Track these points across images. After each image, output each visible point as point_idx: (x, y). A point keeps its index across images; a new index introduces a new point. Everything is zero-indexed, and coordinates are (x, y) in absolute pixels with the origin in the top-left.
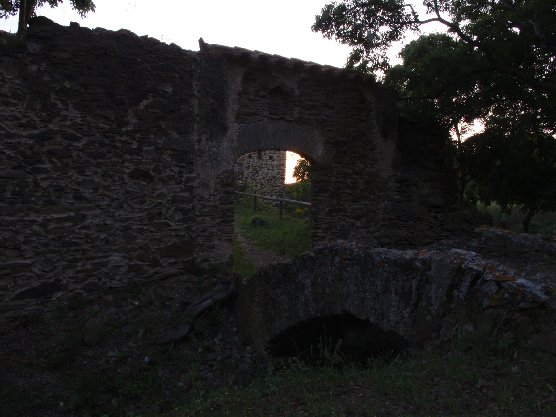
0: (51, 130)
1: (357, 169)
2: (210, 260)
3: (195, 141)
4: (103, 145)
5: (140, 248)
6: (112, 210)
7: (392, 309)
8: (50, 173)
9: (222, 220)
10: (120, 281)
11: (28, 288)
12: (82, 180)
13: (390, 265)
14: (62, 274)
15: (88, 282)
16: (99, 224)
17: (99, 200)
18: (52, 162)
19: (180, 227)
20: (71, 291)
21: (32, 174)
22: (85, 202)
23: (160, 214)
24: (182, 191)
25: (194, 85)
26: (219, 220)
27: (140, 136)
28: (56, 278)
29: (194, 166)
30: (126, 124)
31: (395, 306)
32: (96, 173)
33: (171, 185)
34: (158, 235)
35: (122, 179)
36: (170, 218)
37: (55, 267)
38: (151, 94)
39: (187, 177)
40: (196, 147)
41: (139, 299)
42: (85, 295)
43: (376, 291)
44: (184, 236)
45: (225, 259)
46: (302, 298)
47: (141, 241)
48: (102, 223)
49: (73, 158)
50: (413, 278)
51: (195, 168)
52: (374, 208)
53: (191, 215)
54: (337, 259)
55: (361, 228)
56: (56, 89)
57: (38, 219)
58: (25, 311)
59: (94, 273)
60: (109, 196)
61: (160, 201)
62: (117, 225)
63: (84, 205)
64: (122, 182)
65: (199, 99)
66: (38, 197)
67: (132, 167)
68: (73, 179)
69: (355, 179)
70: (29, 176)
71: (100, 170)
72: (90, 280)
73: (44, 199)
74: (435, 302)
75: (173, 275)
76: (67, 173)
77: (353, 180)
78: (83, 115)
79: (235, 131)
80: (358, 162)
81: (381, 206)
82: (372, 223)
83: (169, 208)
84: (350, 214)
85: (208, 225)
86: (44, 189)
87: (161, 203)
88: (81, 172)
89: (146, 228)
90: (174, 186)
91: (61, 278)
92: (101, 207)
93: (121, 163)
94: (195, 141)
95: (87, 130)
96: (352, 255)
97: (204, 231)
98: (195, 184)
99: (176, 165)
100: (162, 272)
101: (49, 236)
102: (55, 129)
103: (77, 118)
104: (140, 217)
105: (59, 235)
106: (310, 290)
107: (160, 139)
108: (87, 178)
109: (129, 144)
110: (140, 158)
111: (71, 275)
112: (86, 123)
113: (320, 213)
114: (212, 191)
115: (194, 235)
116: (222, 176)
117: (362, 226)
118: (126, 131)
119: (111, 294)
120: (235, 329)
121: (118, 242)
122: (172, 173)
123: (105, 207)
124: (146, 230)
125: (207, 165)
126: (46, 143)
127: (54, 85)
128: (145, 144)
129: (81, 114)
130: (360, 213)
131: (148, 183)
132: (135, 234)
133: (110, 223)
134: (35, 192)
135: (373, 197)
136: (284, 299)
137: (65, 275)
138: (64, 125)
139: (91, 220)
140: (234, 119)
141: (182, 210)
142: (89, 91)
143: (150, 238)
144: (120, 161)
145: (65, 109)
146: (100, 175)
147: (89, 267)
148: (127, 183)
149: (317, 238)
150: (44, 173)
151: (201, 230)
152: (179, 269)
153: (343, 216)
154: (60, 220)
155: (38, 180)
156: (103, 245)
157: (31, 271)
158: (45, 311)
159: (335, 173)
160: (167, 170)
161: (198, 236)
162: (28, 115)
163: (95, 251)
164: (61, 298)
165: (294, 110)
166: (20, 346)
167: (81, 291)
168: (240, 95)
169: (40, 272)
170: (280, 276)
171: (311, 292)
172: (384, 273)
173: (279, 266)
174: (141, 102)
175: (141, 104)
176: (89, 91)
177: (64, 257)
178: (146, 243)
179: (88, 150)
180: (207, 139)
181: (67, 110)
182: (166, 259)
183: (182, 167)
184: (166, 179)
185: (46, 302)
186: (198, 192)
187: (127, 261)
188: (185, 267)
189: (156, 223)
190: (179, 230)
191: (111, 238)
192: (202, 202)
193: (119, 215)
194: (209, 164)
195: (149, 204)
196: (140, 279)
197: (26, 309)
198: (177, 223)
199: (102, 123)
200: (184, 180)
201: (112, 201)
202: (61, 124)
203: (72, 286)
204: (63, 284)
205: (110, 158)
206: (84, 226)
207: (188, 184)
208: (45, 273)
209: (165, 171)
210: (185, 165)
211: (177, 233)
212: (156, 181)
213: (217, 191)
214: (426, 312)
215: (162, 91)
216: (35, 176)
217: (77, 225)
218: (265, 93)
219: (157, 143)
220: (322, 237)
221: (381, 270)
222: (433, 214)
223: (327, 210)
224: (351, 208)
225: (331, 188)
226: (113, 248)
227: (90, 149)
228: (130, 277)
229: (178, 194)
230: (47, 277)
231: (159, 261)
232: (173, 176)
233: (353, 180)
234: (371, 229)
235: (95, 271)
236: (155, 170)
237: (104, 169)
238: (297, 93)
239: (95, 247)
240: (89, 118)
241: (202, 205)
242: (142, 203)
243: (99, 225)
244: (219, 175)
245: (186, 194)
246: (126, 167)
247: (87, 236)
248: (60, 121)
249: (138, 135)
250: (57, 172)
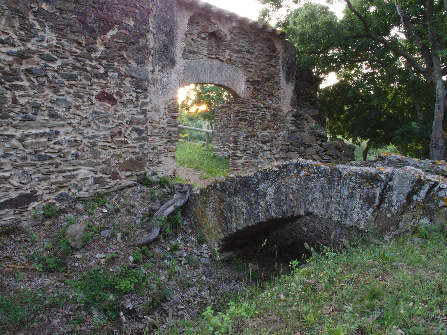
0: (29, 49)
1: (267, 104)
2: (158, 173)
3: (149, 71)
4: (75, 68)
5: (103, 162)
6: (81, 128)
7: (356, 210)
8: (28, 91)
9: (169, 140)
10: (87, 191)
11: (7, 199)
12: (57, 99)
13: (356, 178)
14: (37, 185)
15: (60, 192)
16: (70, 140)
17: (71, 118)
18: (29, 80)
19: (135, 145)
20: (45, 201)
21: (11, 90)
22: (59, 119)
23: (120, 133)
24: (139, 113)
25: (150, 22)
26: (166, 140)
27: (107, 63)
28: (32, 189)
29: (147, 93)
30: (95, 50)
31: (358, 208)
32: (69, 93)
33: (130, 108)
34: (118, 151)
35: (91, 101)
36: (128, 137)
37: (32, 179)
38: (116, 26)
39: (142, 102)
40: (150, 77)
41: (106, 207)
42: (57, 204)
43: (341, 197)
44: (138, 153)
45: (170, 173)
46: (263, 203)
47: (105, 156)
48: (73, 139)
49: (49, 78)
50: (377, 187)
51: (149, 94)
52: (276, 136)
53: (144, 135)
54: (303, 173)
55: (267, 150)
56: (34, 10)
57: (16, 134)
58: (4, 220)
59: (65, 184)
60: (79, 115)
61: (121, 122)
62: (85, 141)
63: (58, 123)
64: (90, 102)
65: (154, 34)
66: (16, 113)
67: (99, 90)
68: (49, 97)
69: (265, 112)
70: (8, 92)
71: (72, 91)
72: (62, 191)
73: (22, 115)
74: (396, 204)
75: (129, 186)
76: (43, 92)
77: (263, 112)
78: (59, 39)
79: (181, 65)
80: (268, 98)
81: (281, 134)
82: (274, 147)
83: (127, 128)
84: (260, 139)
85: (158, 144)
86: (22, 105)
87: (121, 123)
88: (56, 91)
89: (108, 144)
90: (132, 109)
91: (36, 189)
92: (73, 125)
93: (90, 86)
94: (149, 71)
95: (62, 53)
96: (319, 170)
97: (153, 149)
98: (148, 108)
99: (134, 91)
100: (120, 184)
101: (26, 150)
102: (32, 49)
103: (53, 40)
104: (104, 135)
105: (36, 150)
106: (272, 197)
107: (122, 66)
108: (61, 98)
109: (98, 69)
110: (106, 82)
111: (45, 187)
112: (61, 46)
113: (239, 137)
114: (162, 116)
115: (146, 152)
116: (170, 103)
117: (267, 149)
118: (95, 57)
119: (80, 203)
120: (190, 231)
121: (86, 157)
122: (131, 98)
123: (76, 125)
124: (108, 146)
125: (159, 92)
126: (24, 61)
127: (32, 6)
128: (111, 70)
129: (56, 37)
130: (267, 139)
131: (112, 105)
132: (100, 150)
133: (80, 139)
134: (14, 108)
135: (276, 127)
136: (242, 205)
137: (40, 187)
138: (41, 46)
139: (64, 137)
140: (181, 55)
141: (137, 130)
142: (64, 16)
143: (111, 154)
144: (90, 84)
145: (42, 30)
146: (72, 96)
147: (61, 180)
148: (94, 104)
149: (237, 158)
150: (22, 91)
151: (152, 148)
152: (133, 181)
153: (255, 140)
154: (36, 135)
155: (16, 96)
156: (73, 159)
157: (9, 183)
158: (22, 220)
159: (252, 106)
160: (127, 95)
161: (149, 153)
162: (6, 31)
163: (66, 164)
164: (36, 208)
165: (225, 52)
166: (8, 253)
167: (54, 201)
168: (186, 35)
169: (19, 184)
170: (239, 186)
171: (273, 199)
172: (351, 183)
173: (237, 178)
174: (108, 31)
175: (108, 34)
176: (64, 16)
177: (39, 170)
178: (109, 158)
179: (62, 72)
180: (159, 70)
181: (44, 31)
182: (123, 173)
183: (138, 93)
184: (126, 102)
185: (24, 212)
186: (150, 116)
187: (93, 174)
188: (138, 179)
189: (117, 141)
190: (135, 147)
191: (80, 153)
192: (153, 124)
193: (88, 133)
194: (160, 92)
195: (112, 124)
196: (103, 190)
197: (4, 219)
198: (134, 142)
199: (75, 47)
200: (140, 104)
201: (82, 120)
202: (39, 44)
203: (46, 197)
204: (39, 195)
205: (81, 80)
206: (58, 141)
207: (143, 108)
208: (22, 185)
209: (125, 95)
210: (141, 91)
211: (133, 150)
212: (118, 103)
213: (166, 115)
214: (387, 211)
215: (125, 24)
216: (14, 93)
217: (51, 141)
218: (205, 36)
219: (120, 70)
220: (240, 157)
221: (348, 181)
222: (319, 143)
223: (245, 135)
224: (261, 134)
225: (248, 118)
226: (82, 162)
227: (64, 71)
228: (95, 188)
229: (135, 116)
230: (25, 188)
231: (118, 174)
232: (132, 100)
233: (263, 112)
234: (273, 152)
235: (66, 183)
236: (118, 94)
237: (76, 90)
238: (229, 38)
239: (66, 161)
240: (63, 41)
241: (153, 126)
242: (107, 122)
243: (71, 141)
244: (168, 102)
245: (141, 117)
246: (94, 89)
247: (59, 151)
248: (37, 41)
249: (104, 62)
250: (35, 90)
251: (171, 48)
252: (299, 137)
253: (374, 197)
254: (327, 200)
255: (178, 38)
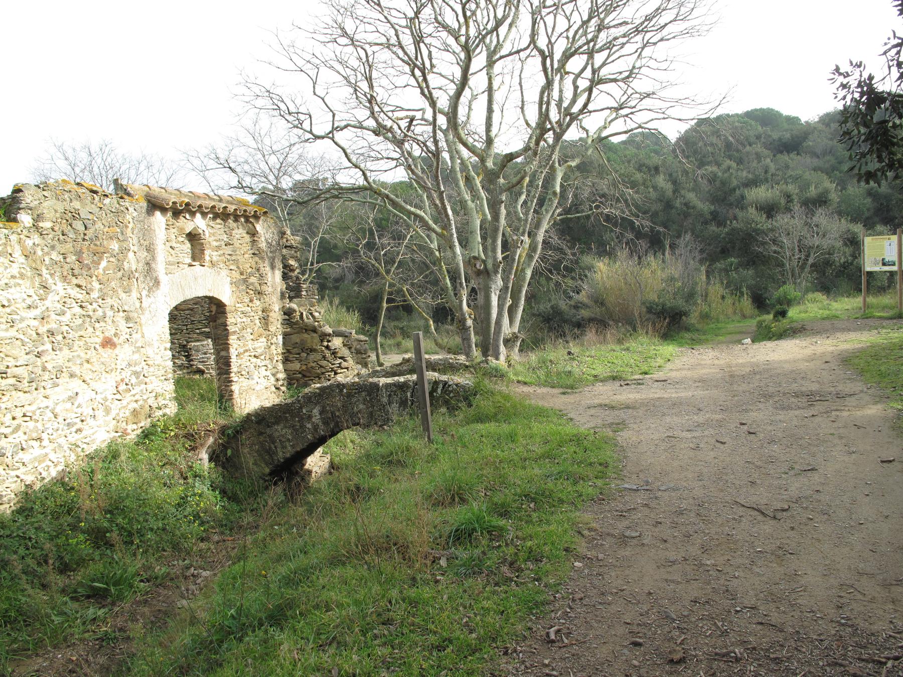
46: (309, 426)
194: (150, 322)
251: (153, 265)
252: (298, 341)
253: (407, 399)
254: (370, 409)
255: (159, 250)
